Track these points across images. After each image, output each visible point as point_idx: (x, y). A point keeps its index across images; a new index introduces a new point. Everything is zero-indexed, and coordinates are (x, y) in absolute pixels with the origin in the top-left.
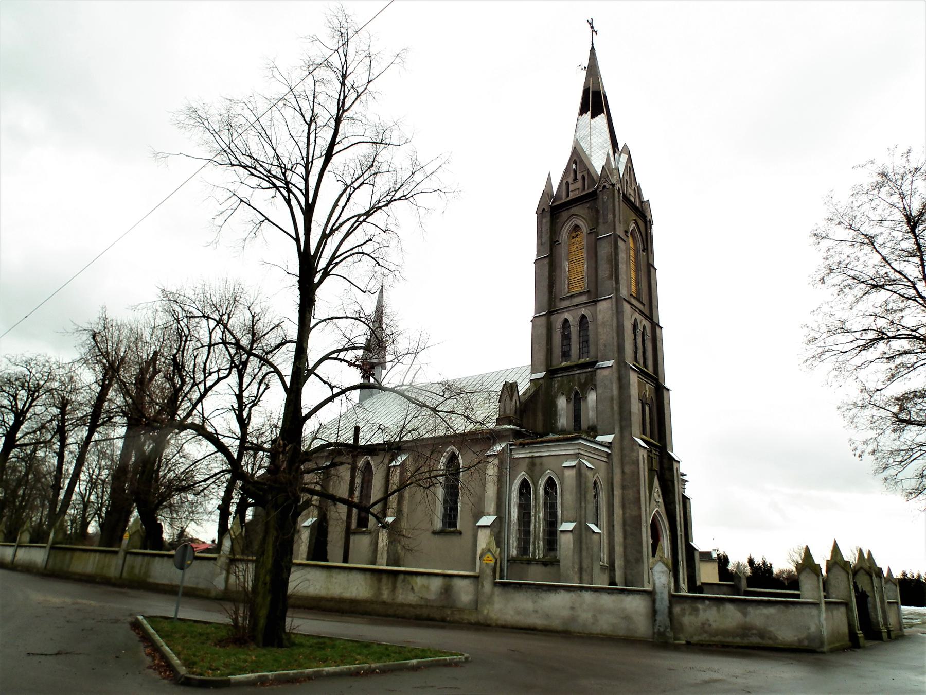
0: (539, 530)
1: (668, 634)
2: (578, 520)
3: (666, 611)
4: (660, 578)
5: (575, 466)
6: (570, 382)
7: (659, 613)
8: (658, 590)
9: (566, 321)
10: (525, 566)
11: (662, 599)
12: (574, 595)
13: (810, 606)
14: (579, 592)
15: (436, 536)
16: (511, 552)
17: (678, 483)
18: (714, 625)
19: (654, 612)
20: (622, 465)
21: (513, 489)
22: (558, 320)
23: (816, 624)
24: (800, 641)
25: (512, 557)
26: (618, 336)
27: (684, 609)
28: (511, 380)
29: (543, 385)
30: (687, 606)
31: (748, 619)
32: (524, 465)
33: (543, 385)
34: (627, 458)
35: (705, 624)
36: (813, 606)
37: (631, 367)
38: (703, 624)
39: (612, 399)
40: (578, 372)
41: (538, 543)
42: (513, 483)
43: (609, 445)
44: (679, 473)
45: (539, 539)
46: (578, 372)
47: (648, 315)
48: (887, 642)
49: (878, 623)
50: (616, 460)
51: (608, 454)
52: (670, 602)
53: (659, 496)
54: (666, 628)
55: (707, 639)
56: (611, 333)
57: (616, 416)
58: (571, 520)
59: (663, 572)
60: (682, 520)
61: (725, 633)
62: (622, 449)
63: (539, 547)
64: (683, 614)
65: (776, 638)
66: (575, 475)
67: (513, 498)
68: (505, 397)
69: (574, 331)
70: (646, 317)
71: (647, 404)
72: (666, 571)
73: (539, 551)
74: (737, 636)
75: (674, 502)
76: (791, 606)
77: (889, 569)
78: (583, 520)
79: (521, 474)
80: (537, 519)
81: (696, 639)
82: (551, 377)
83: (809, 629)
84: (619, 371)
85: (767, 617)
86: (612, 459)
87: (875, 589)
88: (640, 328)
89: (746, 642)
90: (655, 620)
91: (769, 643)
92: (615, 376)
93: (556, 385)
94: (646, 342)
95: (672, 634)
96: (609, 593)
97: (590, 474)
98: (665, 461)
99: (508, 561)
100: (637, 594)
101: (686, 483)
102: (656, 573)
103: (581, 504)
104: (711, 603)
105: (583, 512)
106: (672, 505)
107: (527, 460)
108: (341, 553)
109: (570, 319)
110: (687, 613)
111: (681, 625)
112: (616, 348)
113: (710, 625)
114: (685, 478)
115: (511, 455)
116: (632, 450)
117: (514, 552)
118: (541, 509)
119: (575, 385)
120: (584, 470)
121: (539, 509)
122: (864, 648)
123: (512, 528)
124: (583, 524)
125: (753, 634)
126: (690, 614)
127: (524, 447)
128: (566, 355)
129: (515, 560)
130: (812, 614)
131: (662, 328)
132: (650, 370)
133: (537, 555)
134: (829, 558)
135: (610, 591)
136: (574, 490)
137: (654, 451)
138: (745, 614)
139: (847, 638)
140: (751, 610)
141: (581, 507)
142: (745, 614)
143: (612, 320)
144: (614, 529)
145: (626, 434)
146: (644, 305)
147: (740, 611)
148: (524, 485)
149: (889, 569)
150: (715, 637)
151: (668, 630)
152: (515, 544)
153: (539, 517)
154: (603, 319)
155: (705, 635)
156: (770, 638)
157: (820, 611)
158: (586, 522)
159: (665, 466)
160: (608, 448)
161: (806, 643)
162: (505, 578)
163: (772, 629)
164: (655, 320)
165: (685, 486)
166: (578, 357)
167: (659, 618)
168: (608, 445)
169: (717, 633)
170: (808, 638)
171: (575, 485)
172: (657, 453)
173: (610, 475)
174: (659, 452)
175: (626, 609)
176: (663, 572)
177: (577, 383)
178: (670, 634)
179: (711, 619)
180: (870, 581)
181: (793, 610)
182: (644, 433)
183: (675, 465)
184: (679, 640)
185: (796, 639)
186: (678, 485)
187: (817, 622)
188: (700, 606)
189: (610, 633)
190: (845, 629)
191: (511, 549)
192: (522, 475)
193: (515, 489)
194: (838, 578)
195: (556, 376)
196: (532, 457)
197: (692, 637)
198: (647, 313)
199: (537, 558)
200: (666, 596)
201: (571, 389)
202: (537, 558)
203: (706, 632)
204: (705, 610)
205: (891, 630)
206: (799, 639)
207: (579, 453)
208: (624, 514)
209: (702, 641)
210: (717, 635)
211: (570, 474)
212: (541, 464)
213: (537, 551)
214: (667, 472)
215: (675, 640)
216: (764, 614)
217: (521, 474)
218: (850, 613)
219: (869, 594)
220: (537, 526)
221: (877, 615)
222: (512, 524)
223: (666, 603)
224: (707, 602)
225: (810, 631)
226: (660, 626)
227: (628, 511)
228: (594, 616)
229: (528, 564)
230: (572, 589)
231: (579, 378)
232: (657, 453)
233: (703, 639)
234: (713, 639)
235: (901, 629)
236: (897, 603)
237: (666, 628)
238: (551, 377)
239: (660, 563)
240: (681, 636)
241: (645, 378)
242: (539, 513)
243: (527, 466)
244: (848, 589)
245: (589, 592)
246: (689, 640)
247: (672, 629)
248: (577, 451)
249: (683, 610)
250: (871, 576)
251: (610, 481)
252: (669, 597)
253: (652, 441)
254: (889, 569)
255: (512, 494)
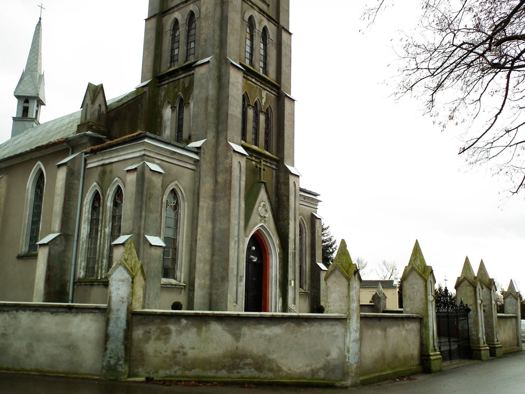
0: (104, 247)
1: (120, 369)
2: (136, 231)
3: (121, 335)
4: (119, 289)
5: (135, 169)
6: (175, 88)
7: (111, 339)
8: (114, 306)
9: (176, 21)
10: (88, 287)
11: (118, 318)
12: (7, 318)
13: (335, 323)
14: (14, 312)
15: (20, 261)
16: (78, 273)
17: (295, 198)
18: (191, 354)
19: (106, 337)
20: (216, 173)
21: (85, 203)
22: (168, 21)
23: (339, 348)
24: (314, 372)
25: (79, 279)
26: (221, 30)
27: (149, 332)
28: (96, 83)
29: (147, 93)
30: (153, 328)
31: (240, 344)
32: (96, 175)
33: (147, 93)
34: (221, 166)
35: (179, 352)
36: (337, 323)
37: (232, 64)
38: (175, 353)
39: (207, 99)
40: (183, 75)
41: (102, 262)
42: (85, 196)
43: (198, 151)
44: (297, 188)
45: (103, 258)
46: (183, 75)
47: (274, 18)
48: (488, 360)
49: (478, 340)
50: (206, 167)
51: (196, 161)
52: (129, 323)
53: (266, 211)
54: (119, 359)
55: (179, 373)
56: (212, 25)
57: (211, 119)
58: (129, 233)
59: (123, 281)
60: (298, 238)
61: (206, 363)
62: (216, 156)
63: (102, 266)
64: (147, 339)
65: (280, 369)
66: (135, 180)
67: (84, 213)
68: (88, 101)
69: (182, 31)
70: (270, 18)
71: (261, 112)
72: (128, 279)
73: (102, 270)
74: (224, 367)
75: (288, 219)
76: (306, 324)
77: (335, 240)
78: (142, 232)
79: (93, 185)
80: (103, 235)
81: (162, 374)
82: (159, 85)
83: (328, 354)
84: (219, 69)
85: (270, 340)
86: (200, 167)
87: (479, 302)
88: (259, 29)
89: (235, 375)
90: (106, 349)
91: (268, 376)
92: (214, 73)
93: (163, 93)
94: (268, 46)
95: (127, 368)
96: (52, 313)
97: (157, 181)
98: (282, 175)
99: (74, 283)
100: (89, 313)
101: (319, 203)
102: (114, 283)
103: (141, 212)
104: (190, 323)
105: (143, 222)
106: (286, 221)
107: (99, 168)
108: (280, 305)
109: (180, 18)
110: (153, 337)
111: (142, 354)
112: (217, 43)
113: (185, 354)
114: (318, 198)
115: (86, 165)
116: (226, 157)
117: (81, 274)
118: (107, 224)
119: (179, 91)
120: (147, 174)
121: (105, 222)
122: (441, 372)
123: (81, 246)
124: (142, 237)
125: (245, 364)
126: (158, 339)
127: (95, 154)
128: (173, 59)
129: (81, 282)
130: (335, 334)
131: (291, 34)
132: (272, 76)
133: (99, 275)
134: (407, 265)
135: (54, 310)
136: (134, 196)
137: (263, 163)
138: (237, 337)
139: (416, 362)
140: (246, 330)
141: (141, 217)
142: (237, 337)
143: (215, 10)
144: (196, 244)
145: (222, 139)
146: (268, 5)
147: (229, 332)
148: (97, 198)
149: (343, 243)
150: (190, 371)
151: (121, 362)
152: (83, 264)
153: (105, 232)
154: (206, 11)
155: (177, 368)
156: (271, 370)
157: (347, 329)
158: (144, 234)
159: (281, 180)
160: (196, 153)
161: (322, 374)
162: (70, 301)
163: (274, 356)
164: (282, 23)
165: (318, 207)
166: (184, 59)
167: (110, 346)
168: (196, 150)
169: (193, 365)
170: (327, 367)
171: (135, 191)
172: (274, 167)
173: (197, 184)
174: (276, 166)
175: (71, 335)
176: (123, 281)
177: (181, 89)
178: (123, 368)
179: (187, 345)
180: (473, 293)
181: (308, 329)
182: (244, 136)
183: (292, 179)
184: (136, 376)
185: (308, 369)
186: (295, 200)
187: (341, 345)
188: (173, 328)
189: (47, 369)
190: (414, 350)
191: (79, 270)
192: (94, 186)
193: (87, 202)
194: (414, 288)
195: (163, 83)
196: (103, 165)
197: (157, 372)
198: (273, 15)
199: (99, 278)
200: (123, 315)
201: (176, 96)
202: (99, 278)
203: (177, 364)
204: (180, 333)
205: (496, 347)
206: (312, 370)
207: (144, 155)
208: (214, 228)
209: (171, 376)
210: (194, 368)
211: (132, 178)
212: (111, 172)
213: (100, 271)
214: (283, 186)
215: (129, 376)
216: (266, 336)
217: (93, 185)
218: (424, 331)
219: (471, 308)
220: (102, 242)
221: (477, 331)
222: (81, 242)
223: (123, 324)
224: (184, 321)
225: (329, 358)
226: (111, 357)
227: (218, 225)
228: (30, 345)
229: (92, 285)
230: (5, 309)
231: (183, 83)
232: (274, 167)
233: (173, 373)
234: (187, 373)
235: (518, 345)
236: (516, 317)
237: (119, 359)
238: (159, 85)
239: (121, 268)
240: (140, 370)
241: (261, 83)
242: (105, 227)
243: (99, 175)
244: (424, 301)
245: (28, 312)
246: (151, 376)
247: (126, 361)
248: (143, 153)
249: (147, 333)
250: (475, 288)
251: (197, 191)
252: (127, 316)
253: (267, 153)
254: (343, 243)
255: (84, 208)
